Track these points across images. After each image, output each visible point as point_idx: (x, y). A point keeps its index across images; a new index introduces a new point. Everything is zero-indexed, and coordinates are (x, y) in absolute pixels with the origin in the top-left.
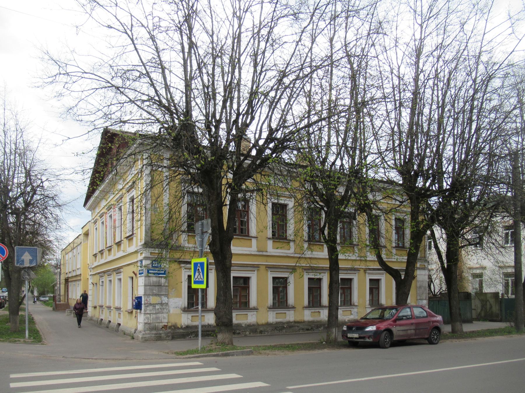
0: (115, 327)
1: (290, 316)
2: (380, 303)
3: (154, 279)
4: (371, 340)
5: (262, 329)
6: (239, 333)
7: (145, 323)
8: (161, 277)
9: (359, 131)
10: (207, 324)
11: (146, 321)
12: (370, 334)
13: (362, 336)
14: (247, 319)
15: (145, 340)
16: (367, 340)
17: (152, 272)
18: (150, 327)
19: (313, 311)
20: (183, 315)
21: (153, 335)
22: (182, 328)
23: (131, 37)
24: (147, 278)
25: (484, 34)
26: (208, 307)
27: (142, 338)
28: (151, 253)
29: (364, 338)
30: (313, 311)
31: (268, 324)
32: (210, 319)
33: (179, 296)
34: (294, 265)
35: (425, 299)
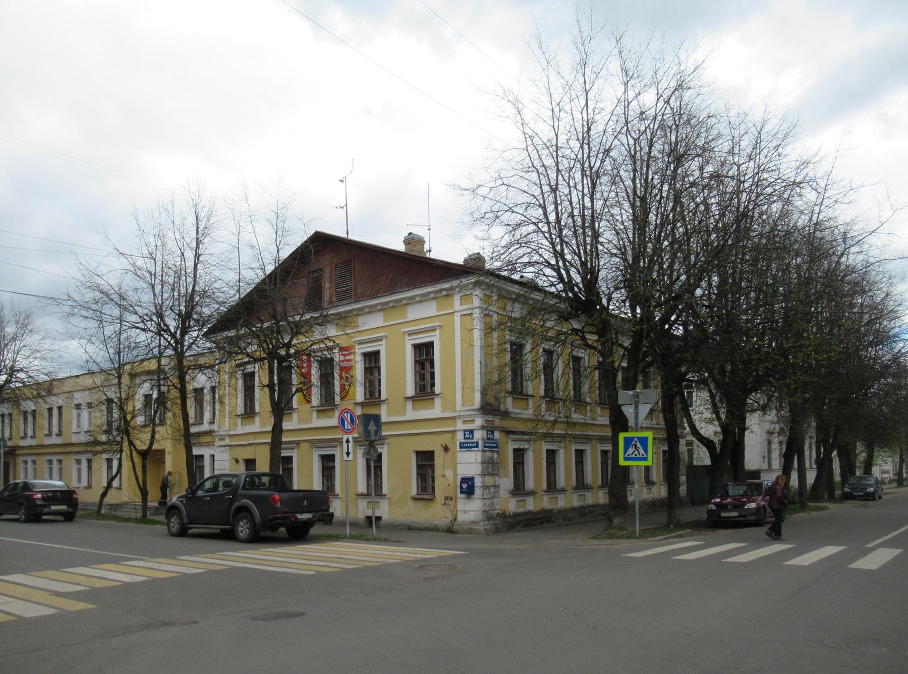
0: (363, 522)
1: (531, 505)
2: (650, 479)
3: (488, 454)
4: (754, 518)
5: (570, 515)
6: (554, 522)
7: (484, 511)
8: (494, 451)
9: (589, 247)
10: (528, 510)
11: (484, 508)
12: (753, 512)
13: (743, 514)
14: (557, 504)
15: (488, 533)
16: (749, 518)
17: (489, 445)
18: (488, 516)
19: (521, 499)
20: (510, 499)
21: (492, 526)
22: (510, 516)
23: (556, 131)
24: (484, 453)
25: (587, 93)
26: (526, 489)
27: (484, 529)
28: (486, 421)
29: (744, 516)
30: (521, 499)
31: (573, 509)
32: (602, 497)
33: (507, 476)
34: (564, 432)
35: (684, 475)
